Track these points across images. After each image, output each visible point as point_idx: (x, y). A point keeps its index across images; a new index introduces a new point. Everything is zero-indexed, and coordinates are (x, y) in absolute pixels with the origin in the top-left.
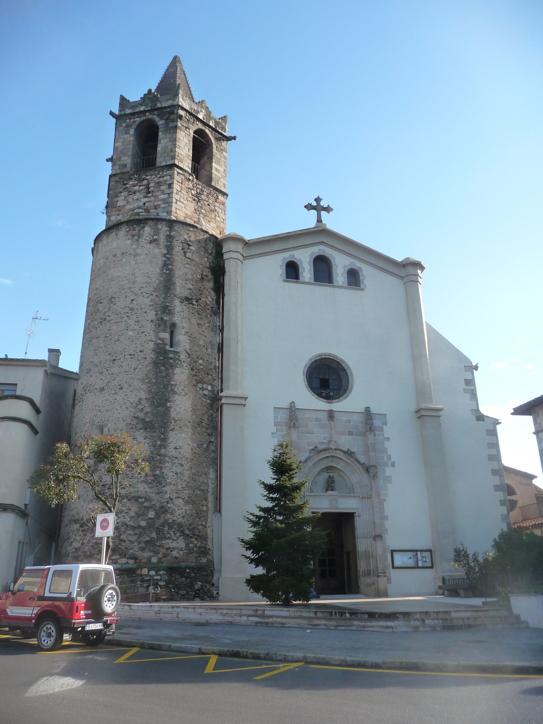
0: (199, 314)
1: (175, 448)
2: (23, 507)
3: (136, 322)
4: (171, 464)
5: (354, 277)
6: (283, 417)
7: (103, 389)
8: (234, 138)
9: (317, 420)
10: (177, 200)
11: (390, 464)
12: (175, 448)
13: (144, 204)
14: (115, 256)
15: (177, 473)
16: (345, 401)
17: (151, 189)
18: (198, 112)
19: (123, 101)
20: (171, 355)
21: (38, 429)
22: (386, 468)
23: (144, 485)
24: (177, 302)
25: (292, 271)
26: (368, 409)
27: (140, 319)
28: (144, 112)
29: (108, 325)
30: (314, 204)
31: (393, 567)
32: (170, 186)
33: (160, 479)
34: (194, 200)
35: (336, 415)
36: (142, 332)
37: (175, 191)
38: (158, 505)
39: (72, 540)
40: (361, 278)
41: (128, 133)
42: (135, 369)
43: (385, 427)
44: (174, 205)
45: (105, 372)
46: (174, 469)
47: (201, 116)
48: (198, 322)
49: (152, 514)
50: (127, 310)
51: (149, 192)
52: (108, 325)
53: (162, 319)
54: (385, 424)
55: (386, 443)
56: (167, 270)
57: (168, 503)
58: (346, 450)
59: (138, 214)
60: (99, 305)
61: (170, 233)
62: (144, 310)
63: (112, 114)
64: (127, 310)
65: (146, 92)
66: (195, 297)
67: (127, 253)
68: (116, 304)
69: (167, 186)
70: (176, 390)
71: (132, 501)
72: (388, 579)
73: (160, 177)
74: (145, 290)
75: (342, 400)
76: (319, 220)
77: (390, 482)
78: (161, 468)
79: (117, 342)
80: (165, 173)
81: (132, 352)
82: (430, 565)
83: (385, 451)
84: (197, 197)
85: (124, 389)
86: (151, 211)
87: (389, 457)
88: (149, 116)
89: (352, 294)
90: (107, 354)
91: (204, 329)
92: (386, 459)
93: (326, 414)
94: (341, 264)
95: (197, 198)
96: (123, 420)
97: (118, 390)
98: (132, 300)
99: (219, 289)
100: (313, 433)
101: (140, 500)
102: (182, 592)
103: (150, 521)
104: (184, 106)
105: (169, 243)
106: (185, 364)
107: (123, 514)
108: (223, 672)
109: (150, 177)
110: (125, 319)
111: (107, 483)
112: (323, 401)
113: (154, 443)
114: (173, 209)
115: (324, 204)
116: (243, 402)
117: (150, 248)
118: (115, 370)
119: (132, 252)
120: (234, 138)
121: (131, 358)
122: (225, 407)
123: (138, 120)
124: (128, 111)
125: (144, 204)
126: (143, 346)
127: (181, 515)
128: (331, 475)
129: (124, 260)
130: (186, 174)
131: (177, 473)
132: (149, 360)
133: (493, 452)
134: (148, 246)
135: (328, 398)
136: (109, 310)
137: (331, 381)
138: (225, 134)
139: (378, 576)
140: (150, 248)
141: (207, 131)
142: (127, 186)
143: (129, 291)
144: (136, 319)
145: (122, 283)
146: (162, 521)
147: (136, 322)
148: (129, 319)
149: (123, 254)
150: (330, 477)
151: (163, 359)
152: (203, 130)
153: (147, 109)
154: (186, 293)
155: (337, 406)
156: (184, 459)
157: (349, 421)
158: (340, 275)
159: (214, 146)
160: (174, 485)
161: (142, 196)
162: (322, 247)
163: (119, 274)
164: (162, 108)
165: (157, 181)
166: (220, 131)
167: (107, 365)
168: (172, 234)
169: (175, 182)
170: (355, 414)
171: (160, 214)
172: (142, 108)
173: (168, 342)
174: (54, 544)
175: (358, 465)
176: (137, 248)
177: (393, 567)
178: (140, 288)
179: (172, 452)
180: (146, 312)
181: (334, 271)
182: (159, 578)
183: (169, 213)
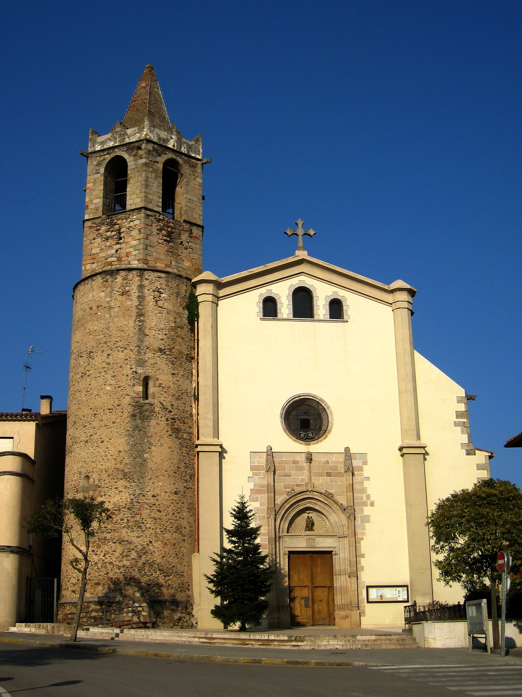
0: (172, 364)
1: (153, 496)
2: (28, 549)
3: (112, 377)
4: (149, 511)
5: (336, 309)
6: (262, 460)
11: (369, 504)
12: (153, 496)
13: (117, 251)
14: (91, 308)
15: (155, 519)
16: (324, 442)
17: (122, 235)
18: (167, 141)
20: (145, 408)
21: (35, 479)
22: (364, 508)
25: (270, 308)
26: (347, 449)
27: (116, 373)
28: (113, 148)
29: (88, 379)
31: (368, 602)
33: (140, 524)
34: (165, 240)
36: (119, 387)
39: (70, 576)
40: (345, 308)
41: (98, 173)
42: (114, 423)
43: (365, 466)
45: (88, 426)
46: (153, 515)
47: (170, 145)
48: (172, 372)
49: (134, 555)
51: (120, 239)
52: (88, 380)
53: (136, 372)
54: (365, 463)
55: (366, 484)
58: (324, 492)
59: (110, 264)
60: (80, 359)
61: (141, 282)
62: (119, 365)
66: (168, 347)
67: (101, 306)
68: (94, 359)
69: (137, 231)
70: (152, 441)
71: (117, 544)
73: (131, 221)
74: (119, 344)
75: (321, 441)
77: (368, 521)
78: (141, 514)
79: (97, 397)
80: (135, 217)
81: (110, 407)
83: (363, 491)
85: (105, 443)
86: (123, 259)
87: (368, 497)
88: (118, 152)
89: (336, 326)
90: (89, 408)
91: (179, 379)
92: (365, 499)
93: (304, 456)
96: (106, 471)
97: (99, 442)
98: (109, 355)
100: (290, 476)
101: (123, 543)
103: (133, 561)
105: (140, 294)
106: (160, 416)
107: (110, 555)
109: (120, 221)
110: (103, 374)
111: (95, 528)
112: (301, 444)
113: (133, 492)
117: (122, 301)
118: (96, 424)
119: (106, 305)
121: (110, 412)
123: (108, 157)
125: (117, 251)
126: (120, 400)
127: (161, 556)
128: (310, 515)
129: (99, 314)
131: (155, 519)
132: (126, 414)
134: (120, 298)
135: (307, 439)
136: (89, 364)
137: (312, 421)
139: (351, 610)
140: (122, 301)
142: (100, 232)
143: (105, 345)
144: (113, 374)
145: (99, 337)
147: (112, 377)
148: (107, 374)
149: (98, 307)
150: (308, 517)
151: (141, 411)
153: (116, 144)
154: (157, 344)
155: (315, 447)
156: (161, 505)
157: (327, 462)
158: (321, 307)
160: (153, 529)
161: (114, 243)
162: (302, 278)
163: (95, 328)
165: (128, 226)
166: (193, 155)
167: (89, 420)
168: (143, 283)
170: (335, 455)
171: (131, 263)
174: (56, 580)
175: (335, 505)
176: (111, 300)
178: (115, 342)
179: (150, 500)
180: (121, 367)
181: (315, 304)
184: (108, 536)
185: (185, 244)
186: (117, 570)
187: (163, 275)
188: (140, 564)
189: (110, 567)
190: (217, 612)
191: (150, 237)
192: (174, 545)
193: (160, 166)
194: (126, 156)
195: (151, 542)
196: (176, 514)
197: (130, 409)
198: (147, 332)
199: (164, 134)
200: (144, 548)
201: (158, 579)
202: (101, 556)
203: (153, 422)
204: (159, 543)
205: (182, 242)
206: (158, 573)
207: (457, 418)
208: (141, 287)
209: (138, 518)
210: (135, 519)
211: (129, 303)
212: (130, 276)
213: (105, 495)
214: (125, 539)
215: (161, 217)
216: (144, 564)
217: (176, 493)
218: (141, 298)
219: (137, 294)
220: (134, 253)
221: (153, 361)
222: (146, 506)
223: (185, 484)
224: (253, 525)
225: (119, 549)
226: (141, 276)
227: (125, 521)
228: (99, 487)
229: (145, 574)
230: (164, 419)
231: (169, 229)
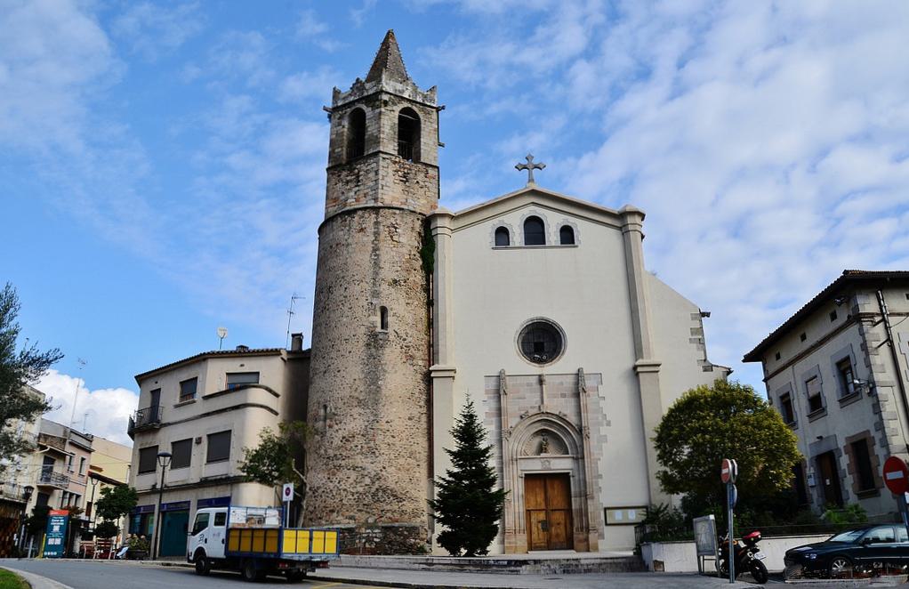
5: (567, 235)
7: (325, 372)
8: (443, 108)
9: (528, 385)
10: (383, 186)
14: (331, 247)
18: (403, 92)
19: (336, 93)
20: (380, 337)
23: (360, 456)
24: (384, 286)
25: (502, 235)
28: (353, 103)
30: (525, 162)
31: (606, 524)
32: (377, 173)
35: (546, 378)
37: (381, 177)
38: (373, 473)
44: (380, 191)
49: (367, 481)
50: (342, 298)
51: (359, 181)
56: (375, 255)
57: (381, 471)
63: (325, 109)
64: (342, 298)
65: (354, 82)
72: (599, 535)
76: (531, 180)
82: (608, 522)
84: (405, 177)
85: (342, 372)
89: (567, 252)
94: (553, 222)
95: (405, 178)
99: (429, 266)
100: (525, 398)
102: (394, 547)
103: (366, 487)
104: (388, 90)
106: (394, 343)
108: (219, 569)
114: (380, 196)
115: (535, 162)
116: (452, 374)
120: (443, 108)
122: (434, 380)
124: (340, 103)
130: (393, 158)
132: (361, 343)
133: (214, 501)
135: (540, 361)
138: (434, 105)
141: (414, 108)
146: (377, 486)
152: (410, 108)
155: (548, 369)
157: (562, 383)
159: (422, 121)
164: (368, 96)
165: (365, 169)
166: (429, 104)
169: (381, 168)
172: (352, 99)
173: (379, 325)
177: (606, 524)
182: (374, 535)
183: (376, 199)
184: (343, 463)
185: (421, 183)
186: (351, 497)
187: (397, 212)
188: (373, 490)
189: (344, 494)
190: (444, 540)
191: (386, 178)
192: (408, 470)
193: (397, 114)
194: (364, 107)
195: (384, 468)
196: (410, 440)
197: (365, 339)
198: (382, 265)
199: (399, 87)
200: (378, 474)
201: (12, 437)
202: (336, 483)
203: (387, 351)
204: (393, 468)
205: (418, 182)
206: (392, 498)
207: (692, 334)
208: (377, 223)
209: (372, 444)
210: (369, 445)
211: (365, 239)
212: (366, 215)
213: (340, 423)
214: (589, 502)
215: (397, 160)
216: (377, 489)
217: (410, 419)
218: (377, 234)
219: (373, 230)
220: (371, 193)
221: (387, 292)
222: (380, 432)
223: (419, 410)
224: (483, 445)
225: (353, 475)
226: (377, 214)
227: (360, 447)
228: (336, 415)
229: (378, 500)
230: (398, 346)
231: (406, 171)
